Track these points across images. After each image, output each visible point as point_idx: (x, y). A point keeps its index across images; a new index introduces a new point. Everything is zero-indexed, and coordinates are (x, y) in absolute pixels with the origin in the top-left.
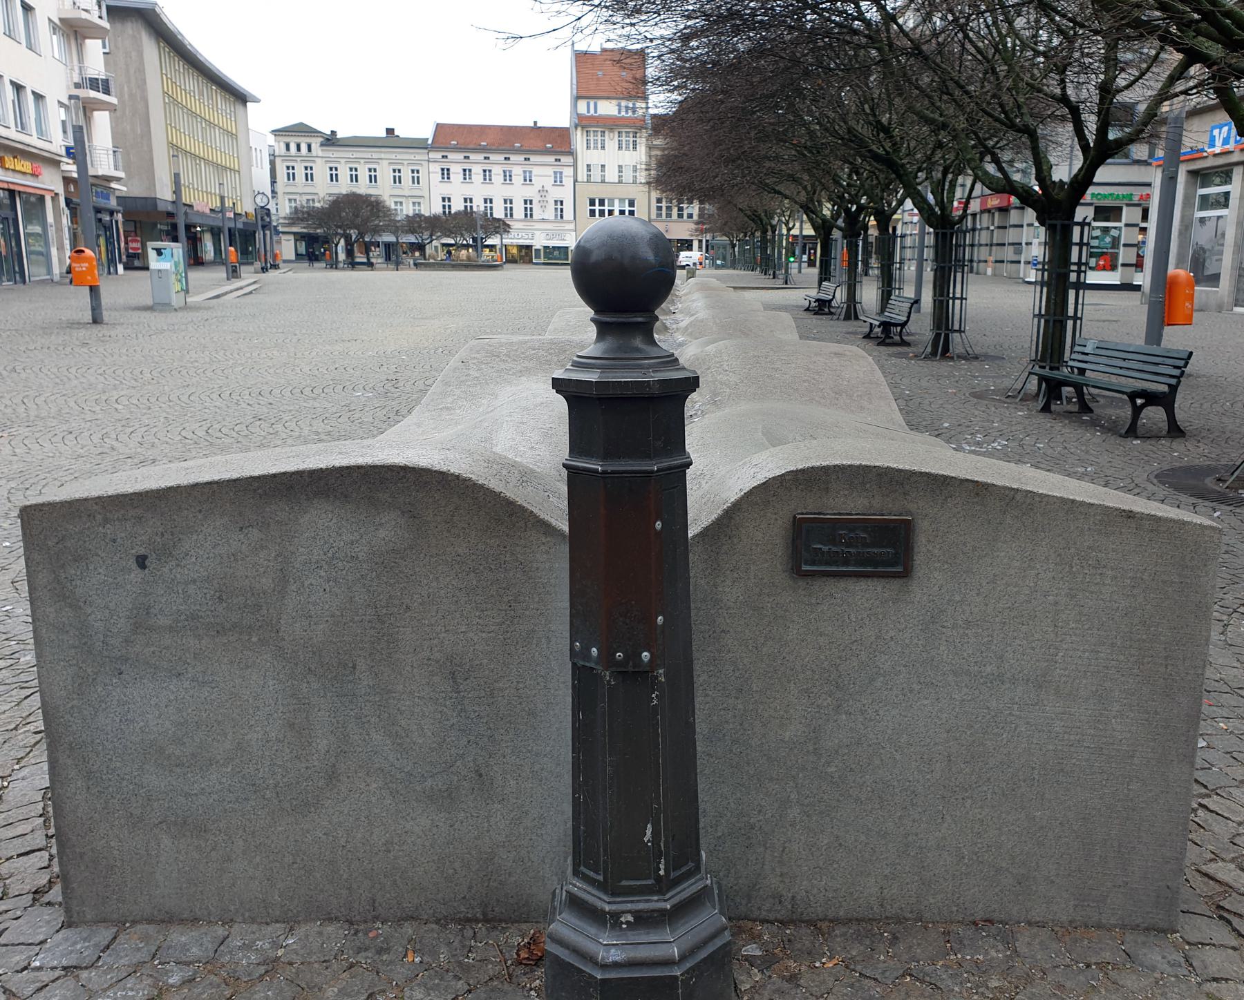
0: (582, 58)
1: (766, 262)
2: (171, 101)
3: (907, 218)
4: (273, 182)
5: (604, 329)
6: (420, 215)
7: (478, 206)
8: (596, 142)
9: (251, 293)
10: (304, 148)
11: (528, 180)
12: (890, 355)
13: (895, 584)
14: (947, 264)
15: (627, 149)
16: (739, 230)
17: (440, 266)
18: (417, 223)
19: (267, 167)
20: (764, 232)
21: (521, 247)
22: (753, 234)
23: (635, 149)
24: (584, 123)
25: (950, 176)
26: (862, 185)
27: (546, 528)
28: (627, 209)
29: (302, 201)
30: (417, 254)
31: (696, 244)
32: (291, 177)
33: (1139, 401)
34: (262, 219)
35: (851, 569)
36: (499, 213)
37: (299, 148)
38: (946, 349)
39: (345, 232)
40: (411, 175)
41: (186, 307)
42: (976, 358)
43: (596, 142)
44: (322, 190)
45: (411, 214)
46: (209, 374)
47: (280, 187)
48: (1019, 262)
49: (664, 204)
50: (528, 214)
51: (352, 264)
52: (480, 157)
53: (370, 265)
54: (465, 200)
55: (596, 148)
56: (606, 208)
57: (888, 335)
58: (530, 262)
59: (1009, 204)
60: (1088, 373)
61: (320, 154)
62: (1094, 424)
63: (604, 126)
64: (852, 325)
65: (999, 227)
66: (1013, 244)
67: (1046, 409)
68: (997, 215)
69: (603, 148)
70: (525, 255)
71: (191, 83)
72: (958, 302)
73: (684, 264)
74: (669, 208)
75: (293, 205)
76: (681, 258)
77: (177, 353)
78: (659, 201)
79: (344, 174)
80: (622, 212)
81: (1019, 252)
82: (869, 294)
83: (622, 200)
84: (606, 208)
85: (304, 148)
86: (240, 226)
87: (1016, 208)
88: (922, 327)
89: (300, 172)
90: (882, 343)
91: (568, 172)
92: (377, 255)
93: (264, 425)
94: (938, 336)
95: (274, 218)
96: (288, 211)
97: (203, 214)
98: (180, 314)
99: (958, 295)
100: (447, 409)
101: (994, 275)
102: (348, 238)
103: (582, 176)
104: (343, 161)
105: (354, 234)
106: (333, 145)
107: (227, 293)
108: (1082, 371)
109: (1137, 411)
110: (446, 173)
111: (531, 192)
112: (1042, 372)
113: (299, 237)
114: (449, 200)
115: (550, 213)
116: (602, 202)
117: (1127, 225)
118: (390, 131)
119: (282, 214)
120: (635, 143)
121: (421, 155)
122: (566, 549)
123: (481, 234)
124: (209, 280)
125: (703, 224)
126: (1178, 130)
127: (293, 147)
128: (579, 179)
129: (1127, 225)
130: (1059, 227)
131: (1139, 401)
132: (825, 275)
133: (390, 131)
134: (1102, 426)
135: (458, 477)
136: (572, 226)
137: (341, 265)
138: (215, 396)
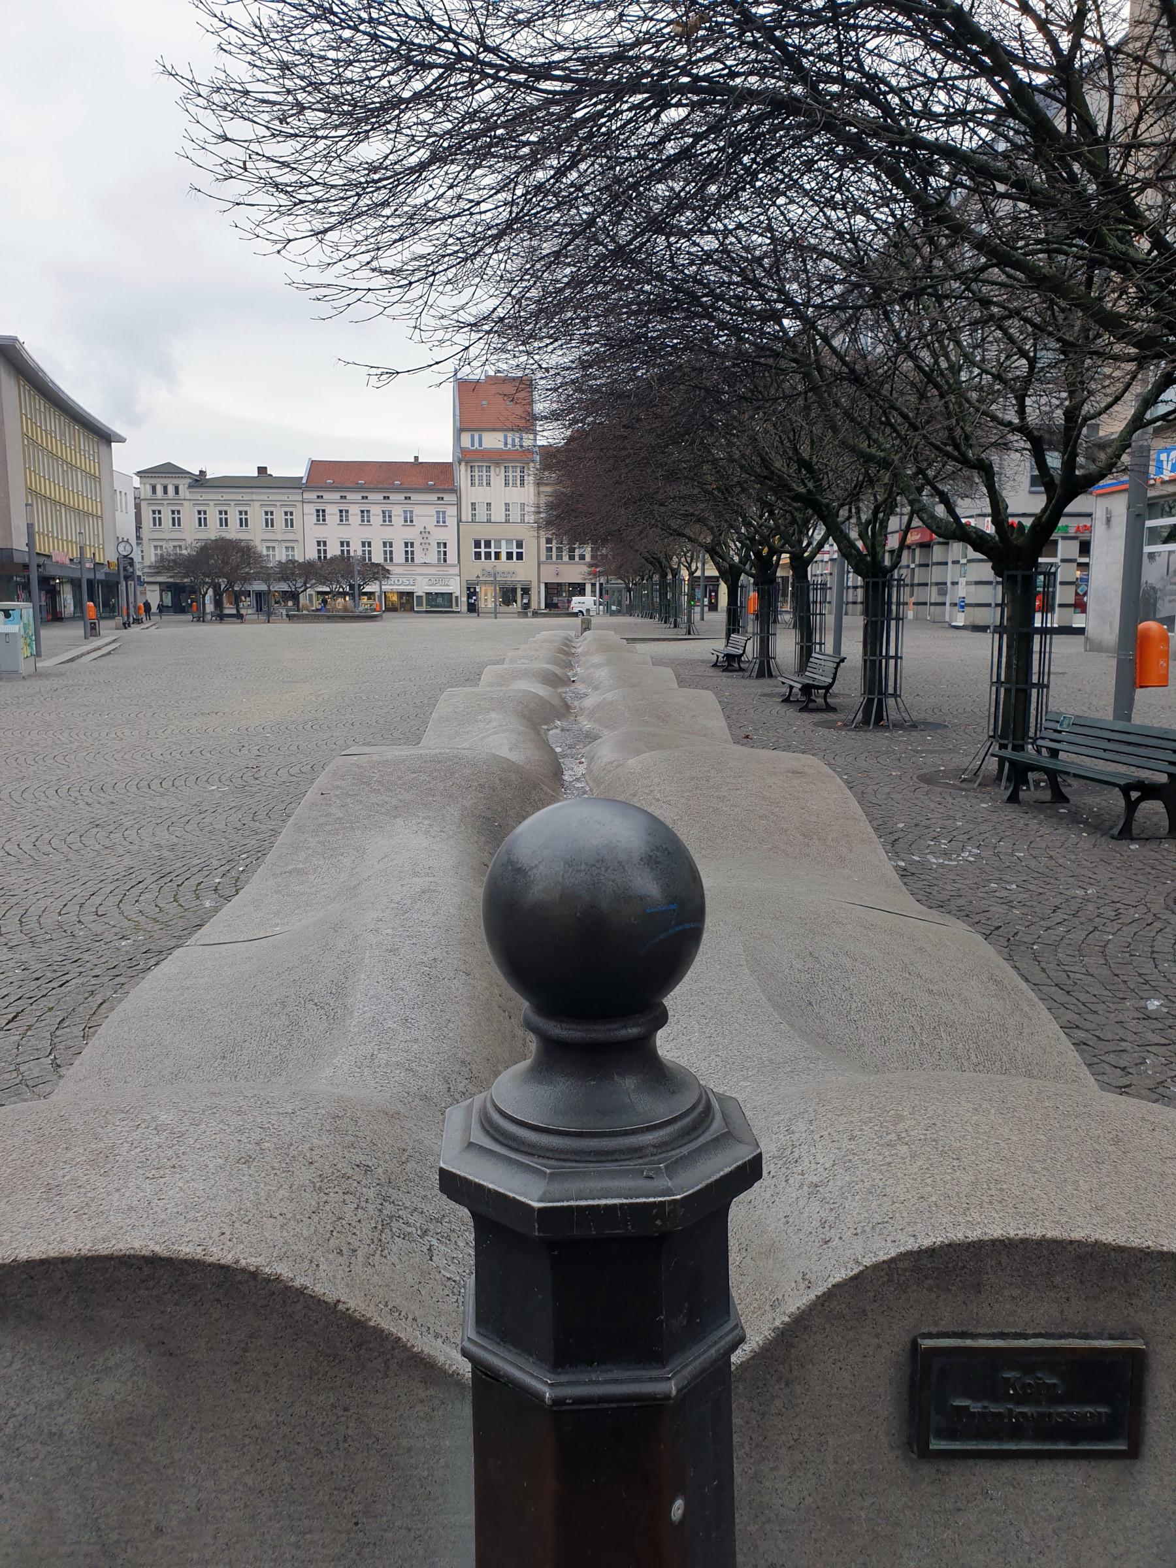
0: (466, 390)
1: (663, 604)
2: (31, 443)
3: (826, 564)
4: (138, 528)
5: (556, 1057)
6: (293, 562)
7: (356, 550)
8: (481, 479)
9: (109, 653)
10: (171, 489)
11: (409, 520)
12: (817, 724)
13: (1109, 1470)
14: (880, 618)
15: (515, 485)
16: (636, 573)
17: (315, 617)
18: (289, 570)
19: (132, 511)
20: (664, 576)
21: (401, 594)
22: (651, 578)
23: (522, 484)
24: (466, 457)
25: (881, 515)
26: (777, 526)
27: (426, 1369)
28: (515, 550)
29: (169, 547)
30: (290, 603)
31: (588, 588)
32: (157, 522)
33: (1135, 795)
34: (125, 569)
35: (1026, 1446)
36: (377, 558)
37: (165, 491)
38: (879, 717)
39: (215, 581)
40: (284, 517)
41: (37, 674)
42: (914, 726)
43: (481, 479)
44: (191, 536)
45: (284, 560)
46: (49, 761)
47: (146, 533)
48: (944, 604)
49: (554, 545)
50: (409, 557)
51: (221, 617)
52: (357, 496)
53: (239, 616)
54: (342, 544)
55: (481, 484)
56: (493, 550)
57: (810, 699)
58: (412, 609)
59: (932, 540)
60: (1062, 755)
61: (188, 496)
62: (1075, 819)
63: (490, 461)
64: (765, 685)
65: (920, 565)
66: (937, 584)
67: (1013, 799)
68: (918, 551)
69: (489, 484)
70: (406, 602)
71: (54, 422)
72: (892, 662)
73: (576, 610)
74: (559, 550)
75: (159, 552)
76: (573, 604)
77: (17, 733)
78: (549, 541)
79: (213, 517)
80: (509, 556)
81: (943, 593)
82: (786, 645)
83: (509, 541)
84: (493, 550)
85: (171, 489)
86: (100, 576)
87: (939, 543)
88: (850, 687)
89: (167, 517)
90: (805, 709)
91: (452, 511)
92: (247, 607)
93: (102, 834)
94: (870, 701)
95: (137, 566)
96: (153, 559)
97: (61, 566)
98: (28, 683)
99: (892, 653)
100: (299, 872)
101: (916, 618)
102: (216, 588)
103: (466, 515)
104: (212, 503)
105: (223, 583)
106: (202, 486)
107: (83, 655)
108: (1054, 753)
109: (1131, 806)
110: (321, 515)
111: (411, 534)
112: (1003, 753)
113: (165, 587)
114: (325, 543)
115: (432, 557)
116: (488, 544)
117: (1063, 561)
118: (262, 470)
119: (147, 563)
120: (522, 481)
121: (295, 496)
122: (465, 1411)
123: (358, 581)
124: (64, 639)
125: (597, 566)
126: (1143, 461)
127: (159, 489)
128: (464, 519)
129: (1063, 561)
130: (1019, 578)
131: (1135, 795)
132: (734, 623)
133: (262, 470)
134: (1086, 822)
135: (254, 1275)
136: (456, 570)
137: (209, 617)
138: (51, 792)
